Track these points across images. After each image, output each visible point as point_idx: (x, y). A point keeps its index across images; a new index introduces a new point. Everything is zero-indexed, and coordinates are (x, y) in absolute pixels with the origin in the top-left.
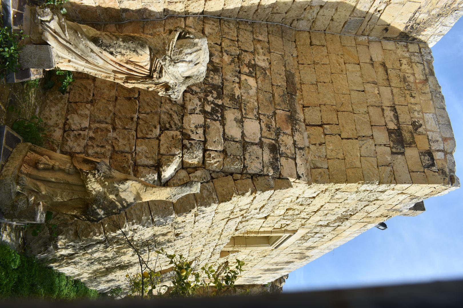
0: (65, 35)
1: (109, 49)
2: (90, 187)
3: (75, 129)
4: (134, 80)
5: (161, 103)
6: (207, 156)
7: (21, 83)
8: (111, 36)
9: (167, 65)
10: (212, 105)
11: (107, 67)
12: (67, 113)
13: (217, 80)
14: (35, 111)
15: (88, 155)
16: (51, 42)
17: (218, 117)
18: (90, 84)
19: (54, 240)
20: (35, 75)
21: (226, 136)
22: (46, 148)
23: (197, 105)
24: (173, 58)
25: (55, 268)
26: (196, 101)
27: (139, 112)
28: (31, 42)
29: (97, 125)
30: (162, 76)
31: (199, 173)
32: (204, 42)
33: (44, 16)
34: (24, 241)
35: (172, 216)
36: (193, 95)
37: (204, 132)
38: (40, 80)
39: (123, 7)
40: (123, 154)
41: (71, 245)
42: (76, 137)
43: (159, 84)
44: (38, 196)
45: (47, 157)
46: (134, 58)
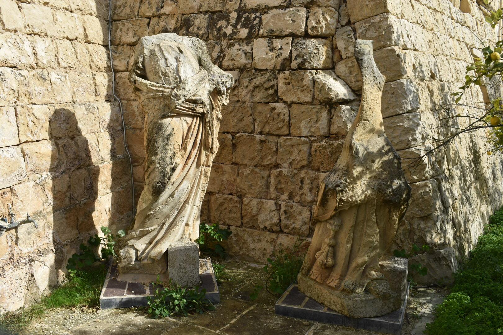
0: (152, 230)
1: (168, 173)
2: (360, 198)
3: (278, 218)
4: (208, 139)
5: (238, 101)
6: (315, 33)
7: (218, 285)
8: (149, 171)
9: (184, 93)
10: (239, 27)
11: (192, 175)
12: (256, 229)
13: (201, 21)
14: (255, 268)
15: (314, 201)
16: (163, 247)
17: (256, 17)
18: (217, 198)
19: (432, 248)
20: (207, 268)
21: (285, 4)
22: (305, 255)
23: (239, 50)
24: (173, 85)
25: (472, 249)
26: (234, 51)
27: (253, 132)
28: (165, 273)
29: (272, 189)
30: (201, 100)
31: (341, 45)
32: (148, 41)
33: (131, 258)
34: (431, 287)
35: (405, 83)
36: (224, 55)
37: (279, 37)
38: (213, 262)
39: (109, 157)
40: (313, 153)
41: (441, 226)
42: (289, 217)
43: (211, 105)
44: (371, 266)
45: (317, 254)
46: (178, 139)
